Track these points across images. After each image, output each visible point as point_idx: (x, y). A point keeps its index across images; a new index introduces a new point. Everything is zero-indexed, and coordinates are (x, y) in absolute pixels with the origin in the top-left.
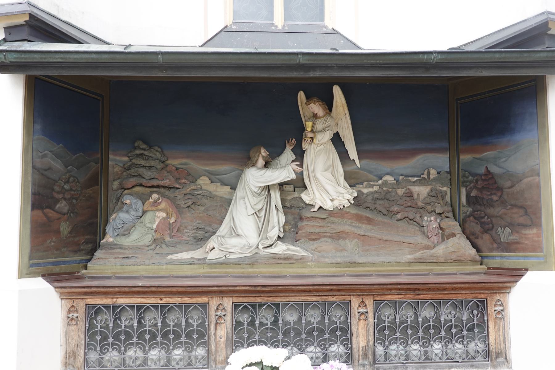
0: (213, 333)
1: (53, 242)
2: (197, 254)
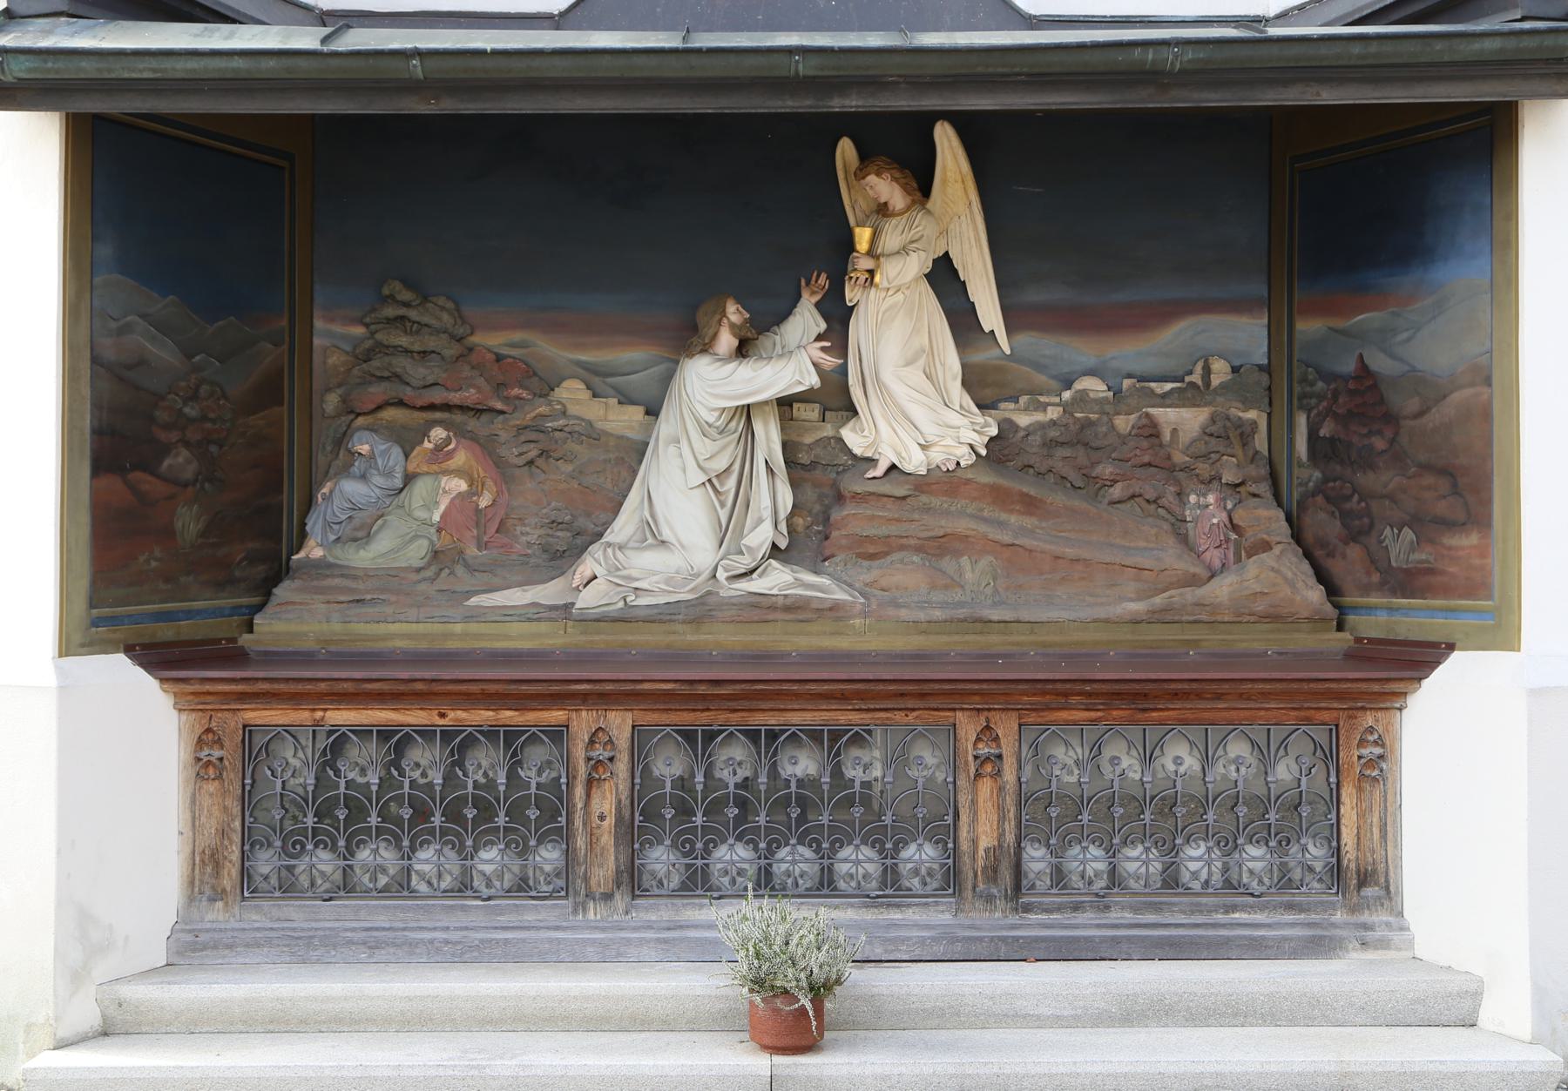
0: (580, 806)
1: (156, 560)
2: (547, 593)
